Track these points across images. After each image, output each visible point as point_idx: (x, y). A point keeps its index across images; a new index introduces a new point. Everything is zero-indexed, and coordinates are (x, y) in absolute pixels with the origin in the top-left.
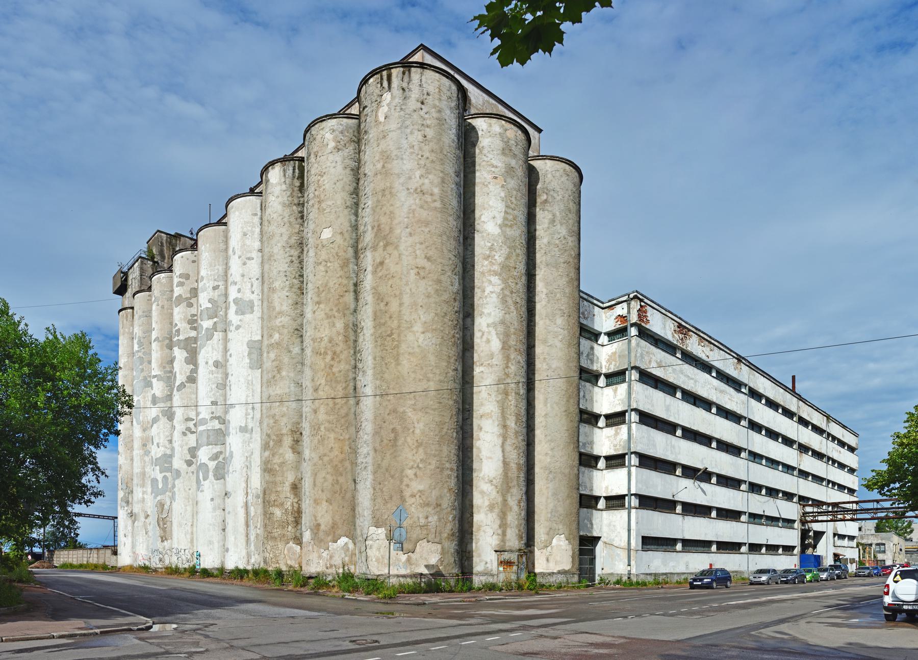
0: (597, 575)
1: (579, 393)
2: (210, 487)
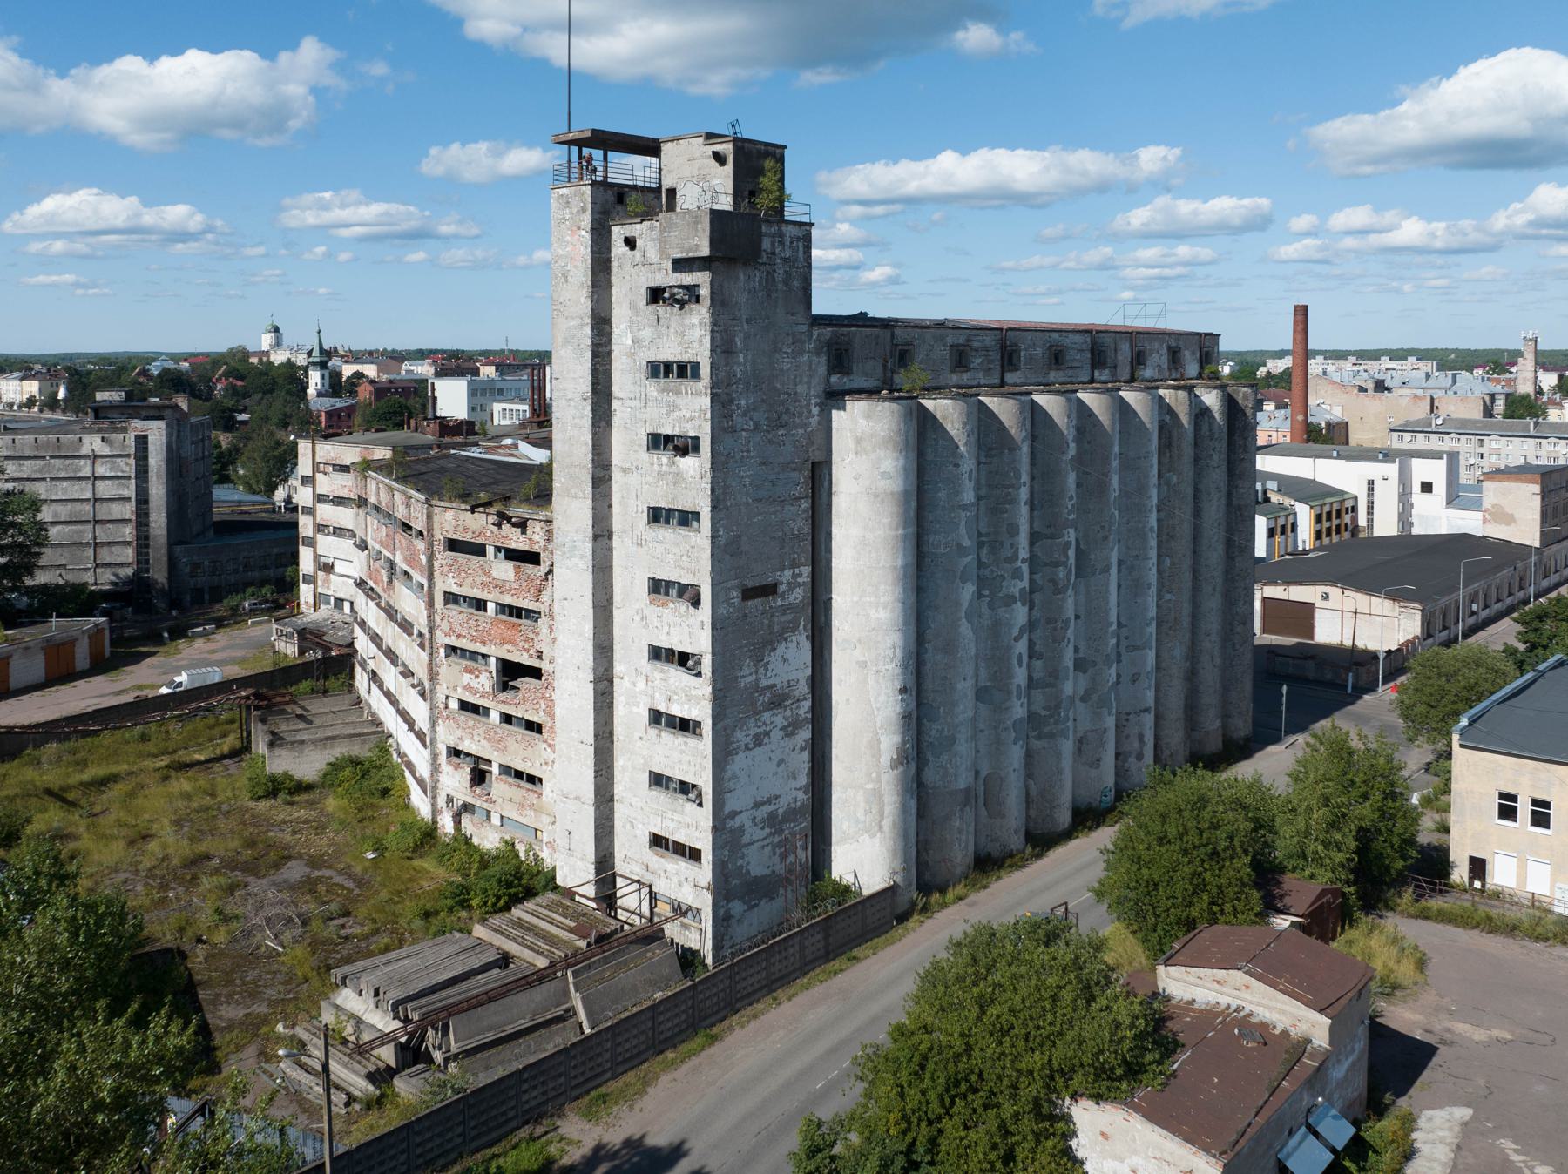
0: (592, 150)
1: (199, 763)
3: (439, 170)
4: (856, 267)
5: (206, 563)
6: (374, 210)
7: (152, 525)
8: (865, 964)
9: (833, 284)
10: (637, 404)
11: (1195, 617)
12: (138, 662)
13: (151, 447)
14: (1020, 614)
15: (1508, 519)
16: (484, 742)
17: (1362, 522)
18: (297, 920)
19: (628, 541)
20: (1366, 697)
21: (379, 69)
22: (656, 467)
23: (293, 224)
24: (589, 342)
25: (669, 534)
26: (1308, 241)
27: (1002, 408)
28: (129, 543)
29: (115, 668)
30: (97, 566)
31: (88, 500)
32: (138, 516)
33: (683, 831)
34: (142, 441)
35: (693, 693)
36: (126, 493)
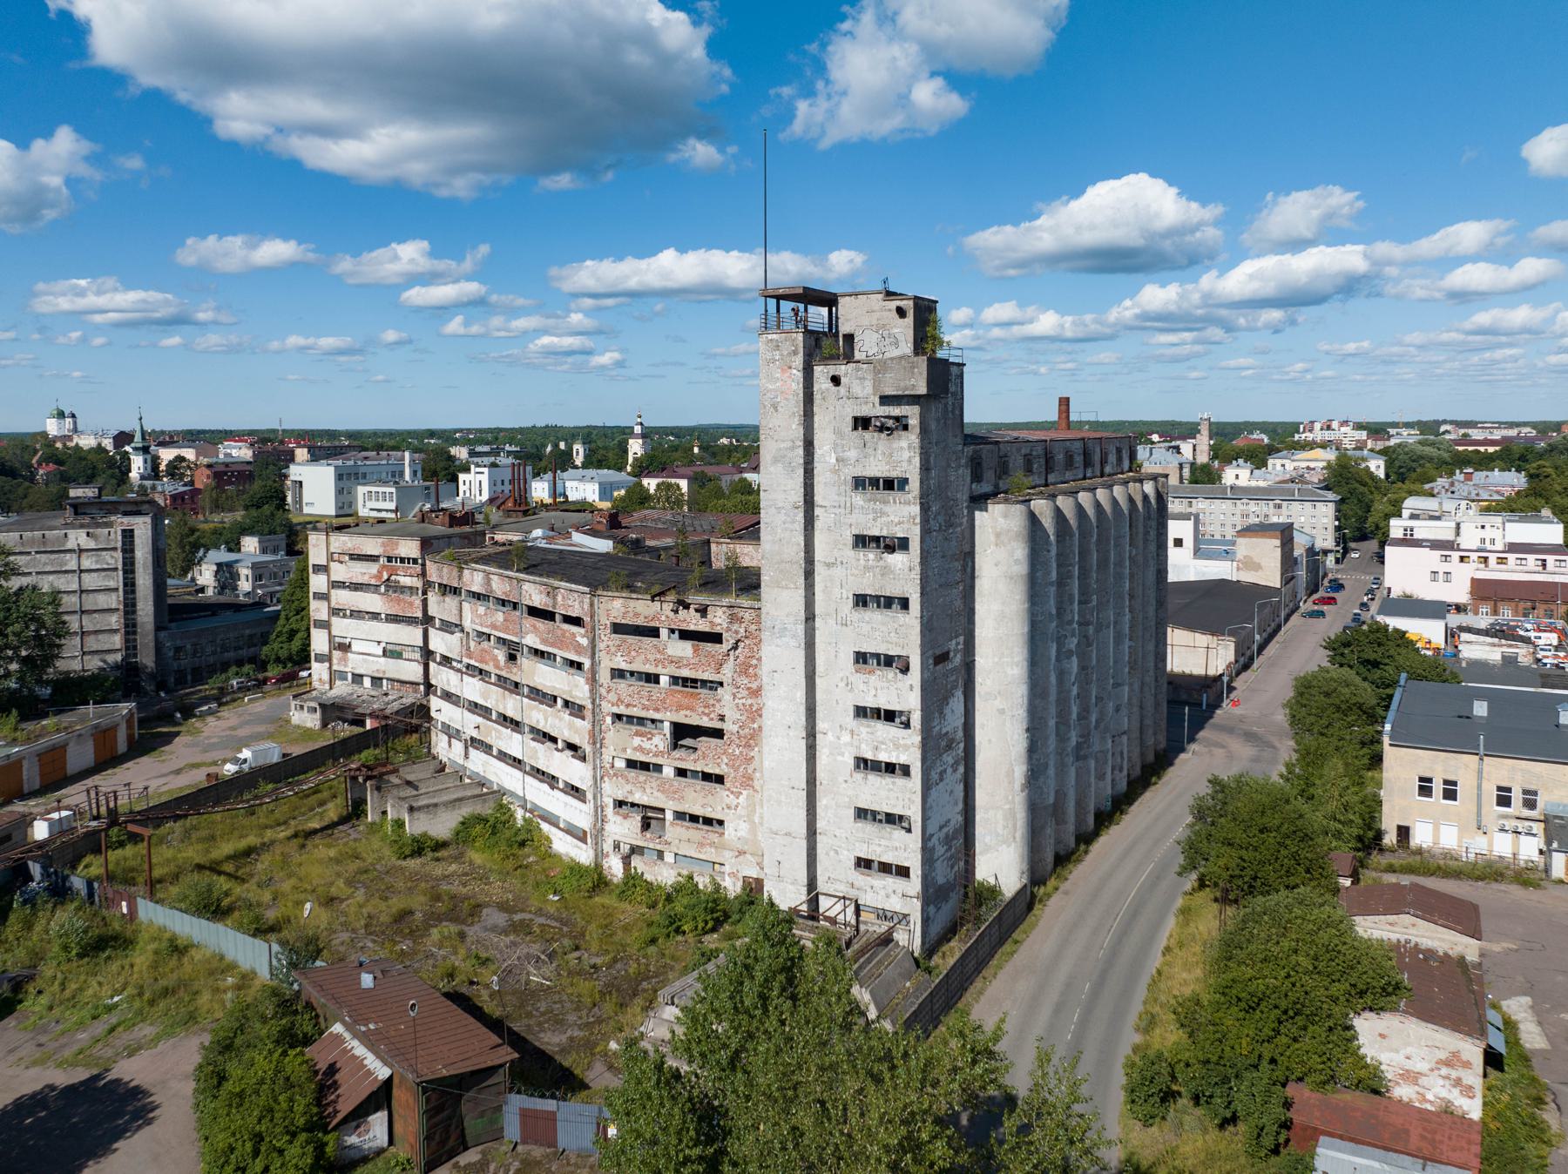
3: (191, 260)
4: (588, 352)
5: (189, 646)
6: (133, 297)
7: (139, 613)
8: (1025, 944)
9: (565, 367)
10: (842, 510)
12: (169, 742)
13: (137, 541)
15: (1256, 567)
16: (659, 794)
18: (543, 957)
19: (832, 622)
20: (1218, 712)
21: (135, 163)
22: (862, 562)
23: (44, 309)
24: (802, 461)
26: (967, 332)
28: (115, 631)
29: (154, 749)
30: (84, 653)
31: (75, 592)
32: (126, 605)
33: (890, 854)
34: (128, 535)
35: (901, 742)
36: (112, 584)
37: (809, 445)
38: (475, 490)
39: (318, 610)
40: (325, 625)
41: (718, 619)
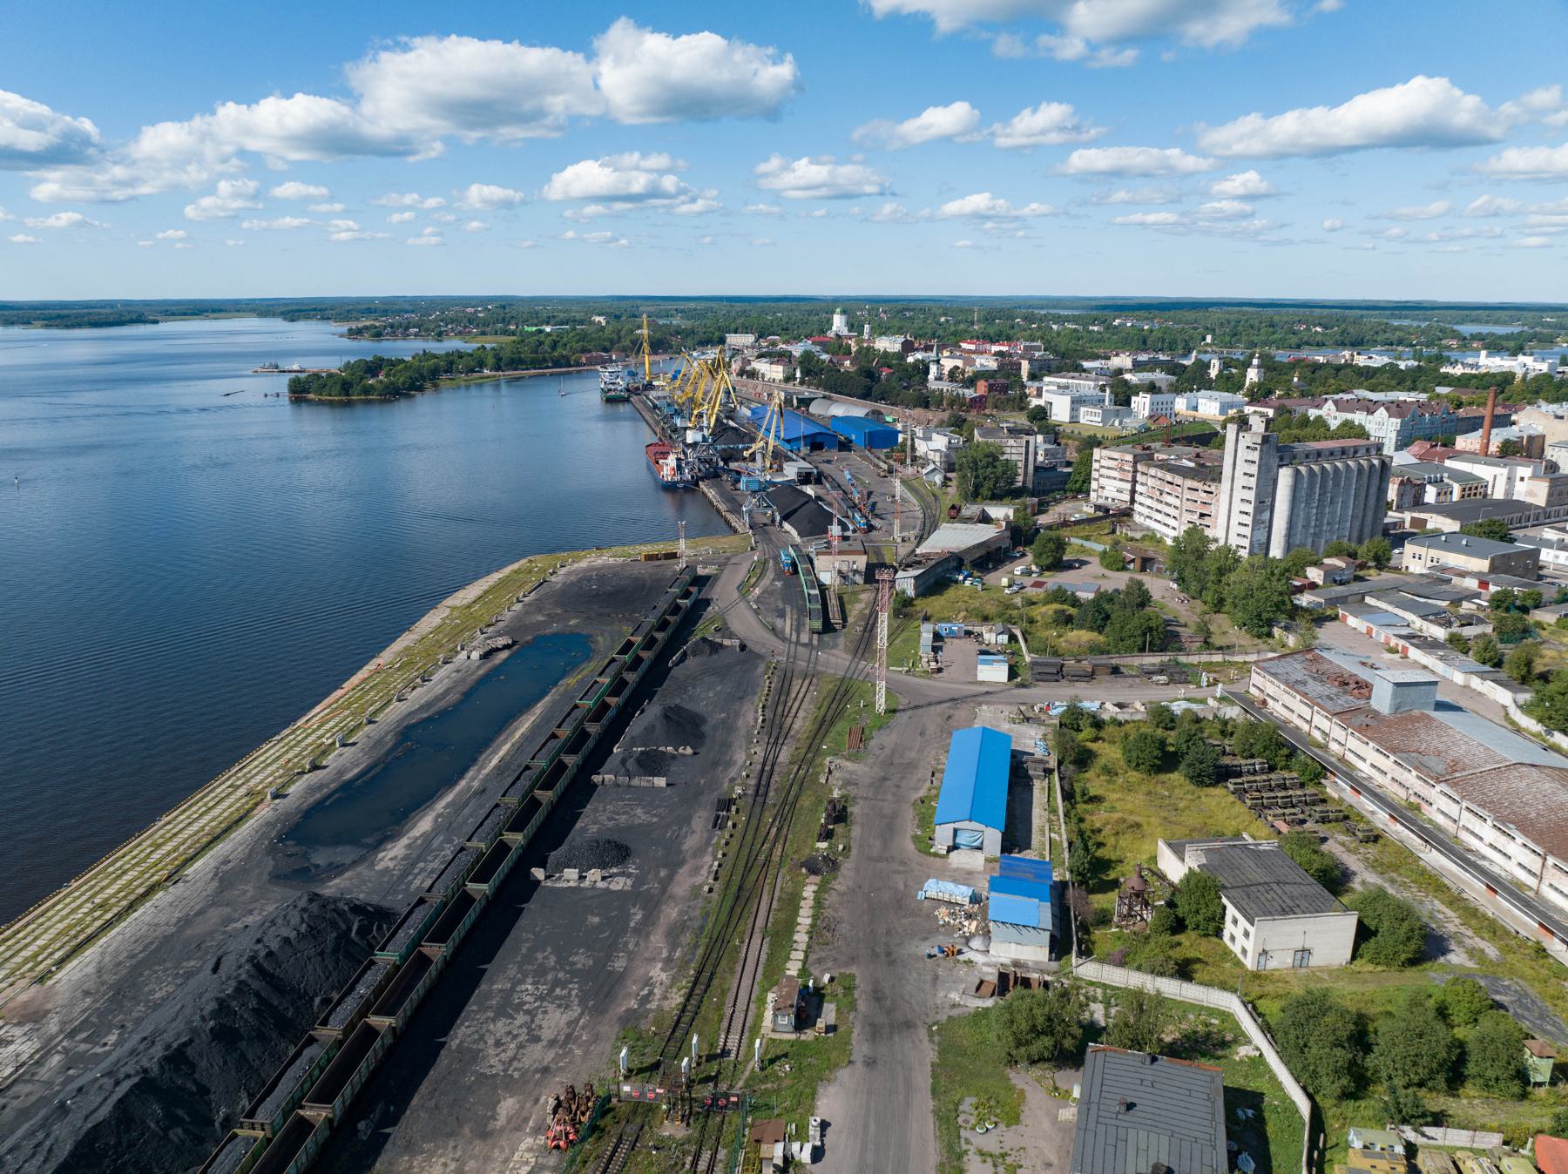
2: (1193, 1093)
11: (1364, 516)
14: (1315, 511)
17: (1489, 492)
25: (1246, 491)
27: (1316, 468)
34: (1028, 442)
37: (1236, 451)
38: (1141, 407)
39: (1095, 475)
40: (1097, 480)
41: (1213, 489)
